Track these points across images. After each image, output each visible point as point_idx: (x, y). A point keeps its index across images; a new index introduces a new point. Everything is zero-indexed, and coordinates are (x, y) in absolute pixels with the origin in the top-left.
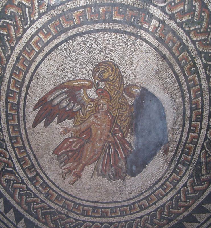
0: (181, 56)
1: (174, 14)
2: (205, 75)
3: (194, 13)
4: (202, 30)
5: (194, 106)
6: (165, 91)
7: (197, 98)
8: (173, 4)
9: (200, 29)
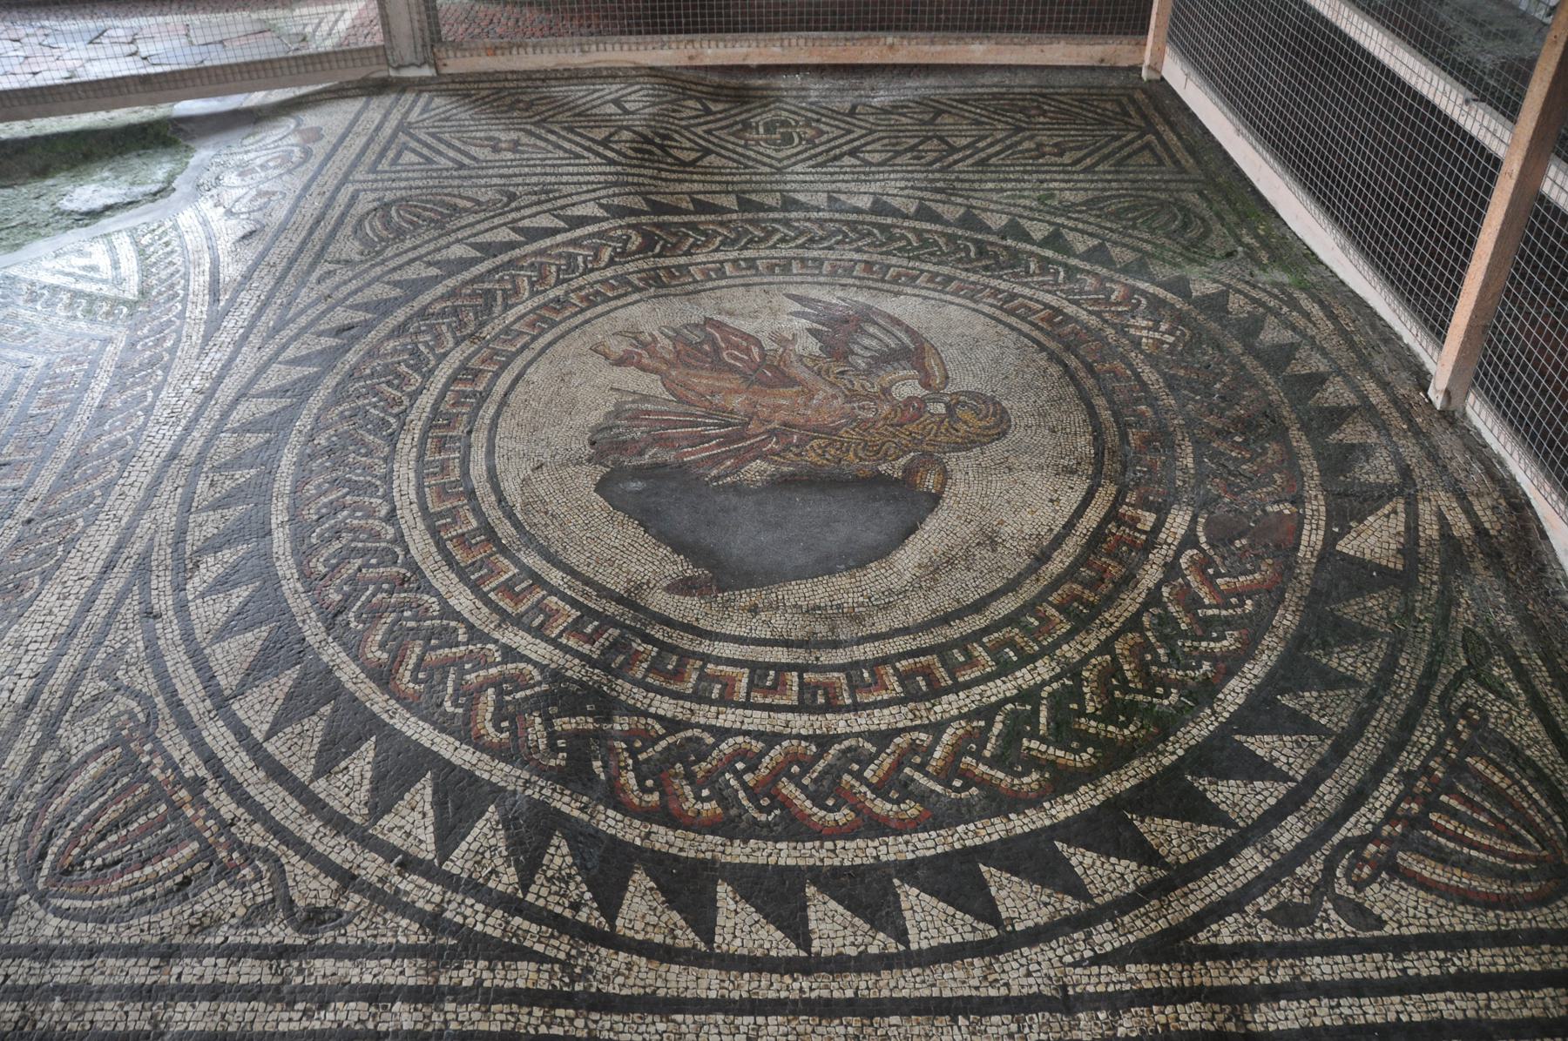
0: (1051, 611)
1: (1184, 577)
2: (993, 699)
3: (1201, 639)
4: (1154, 669)
5: (866, 675)
6: (926, 567)
7: (902, 684)
8: (1211, 571)
9: (1156, 660)
